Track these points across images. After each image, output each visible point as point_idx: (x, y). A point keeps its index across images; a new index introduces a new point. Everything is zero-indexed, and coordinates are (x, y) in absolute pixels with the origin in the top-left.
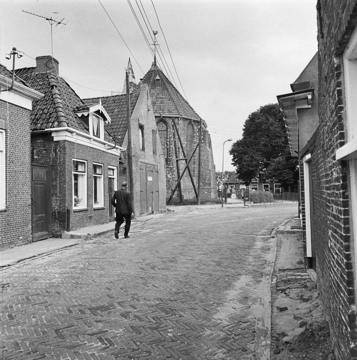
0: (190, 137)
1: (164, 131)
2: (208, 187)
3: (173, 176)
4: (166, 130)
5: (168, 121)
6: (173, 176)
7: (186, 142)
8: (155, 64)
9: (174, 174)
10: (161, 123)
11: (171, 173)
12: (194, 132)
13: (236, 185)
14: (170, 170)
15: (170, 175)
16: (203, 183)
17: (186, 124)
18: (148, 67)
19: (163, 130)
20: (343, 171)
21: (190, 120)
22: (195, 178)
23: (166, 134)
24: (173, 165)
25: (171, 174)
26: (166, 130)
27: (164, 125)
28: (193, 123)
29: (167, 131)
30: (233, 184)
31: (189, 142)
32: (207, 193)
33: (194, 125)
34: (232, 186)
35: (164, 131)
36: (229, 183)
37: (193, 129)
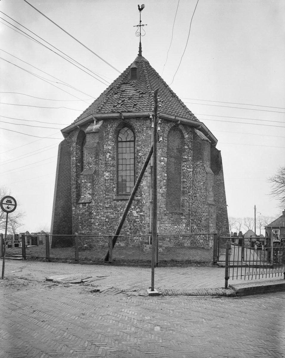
0: (175, 151)
1: (130, 141)
2: (205, 232)
3: (142, 214)
4: (133, 139)
5: (134, 125)
6: (142, 214)
7: (166, 159)
8: (140, 55)
9: (143, 209)
10: (126, 129)
11: (139, 208)
12: (183, 143)
13: (281, 229)
14: (137, 205)
15: (137, 212)
16: (197, 226)
17: (167, 129)
18: (130, 60)
19: (128, 140)
20: (241, 243)
21: (176, 121)
22: (184, 217)
23: (133, 146)
24: (141, 196)
25: (138, 210)
26: (133, 139)
27: (129, 132)
28: (181, 127)
29: (134, 141)
30: (278, 228)
31: (173, 160)
32: (202, 241)
33: (184, 132)
34: (276, 231)
35: (130, 141)
36: (272, 227)
37: (183, 137)
